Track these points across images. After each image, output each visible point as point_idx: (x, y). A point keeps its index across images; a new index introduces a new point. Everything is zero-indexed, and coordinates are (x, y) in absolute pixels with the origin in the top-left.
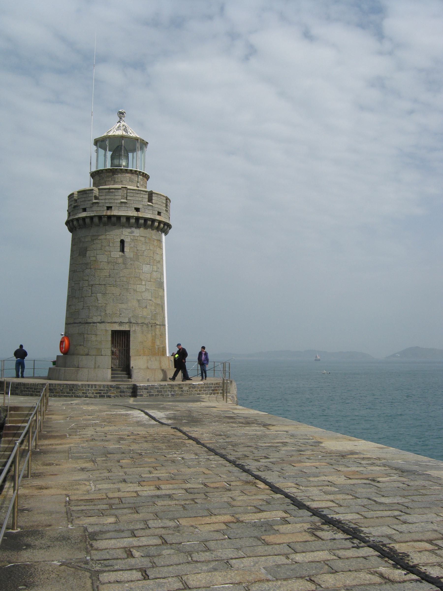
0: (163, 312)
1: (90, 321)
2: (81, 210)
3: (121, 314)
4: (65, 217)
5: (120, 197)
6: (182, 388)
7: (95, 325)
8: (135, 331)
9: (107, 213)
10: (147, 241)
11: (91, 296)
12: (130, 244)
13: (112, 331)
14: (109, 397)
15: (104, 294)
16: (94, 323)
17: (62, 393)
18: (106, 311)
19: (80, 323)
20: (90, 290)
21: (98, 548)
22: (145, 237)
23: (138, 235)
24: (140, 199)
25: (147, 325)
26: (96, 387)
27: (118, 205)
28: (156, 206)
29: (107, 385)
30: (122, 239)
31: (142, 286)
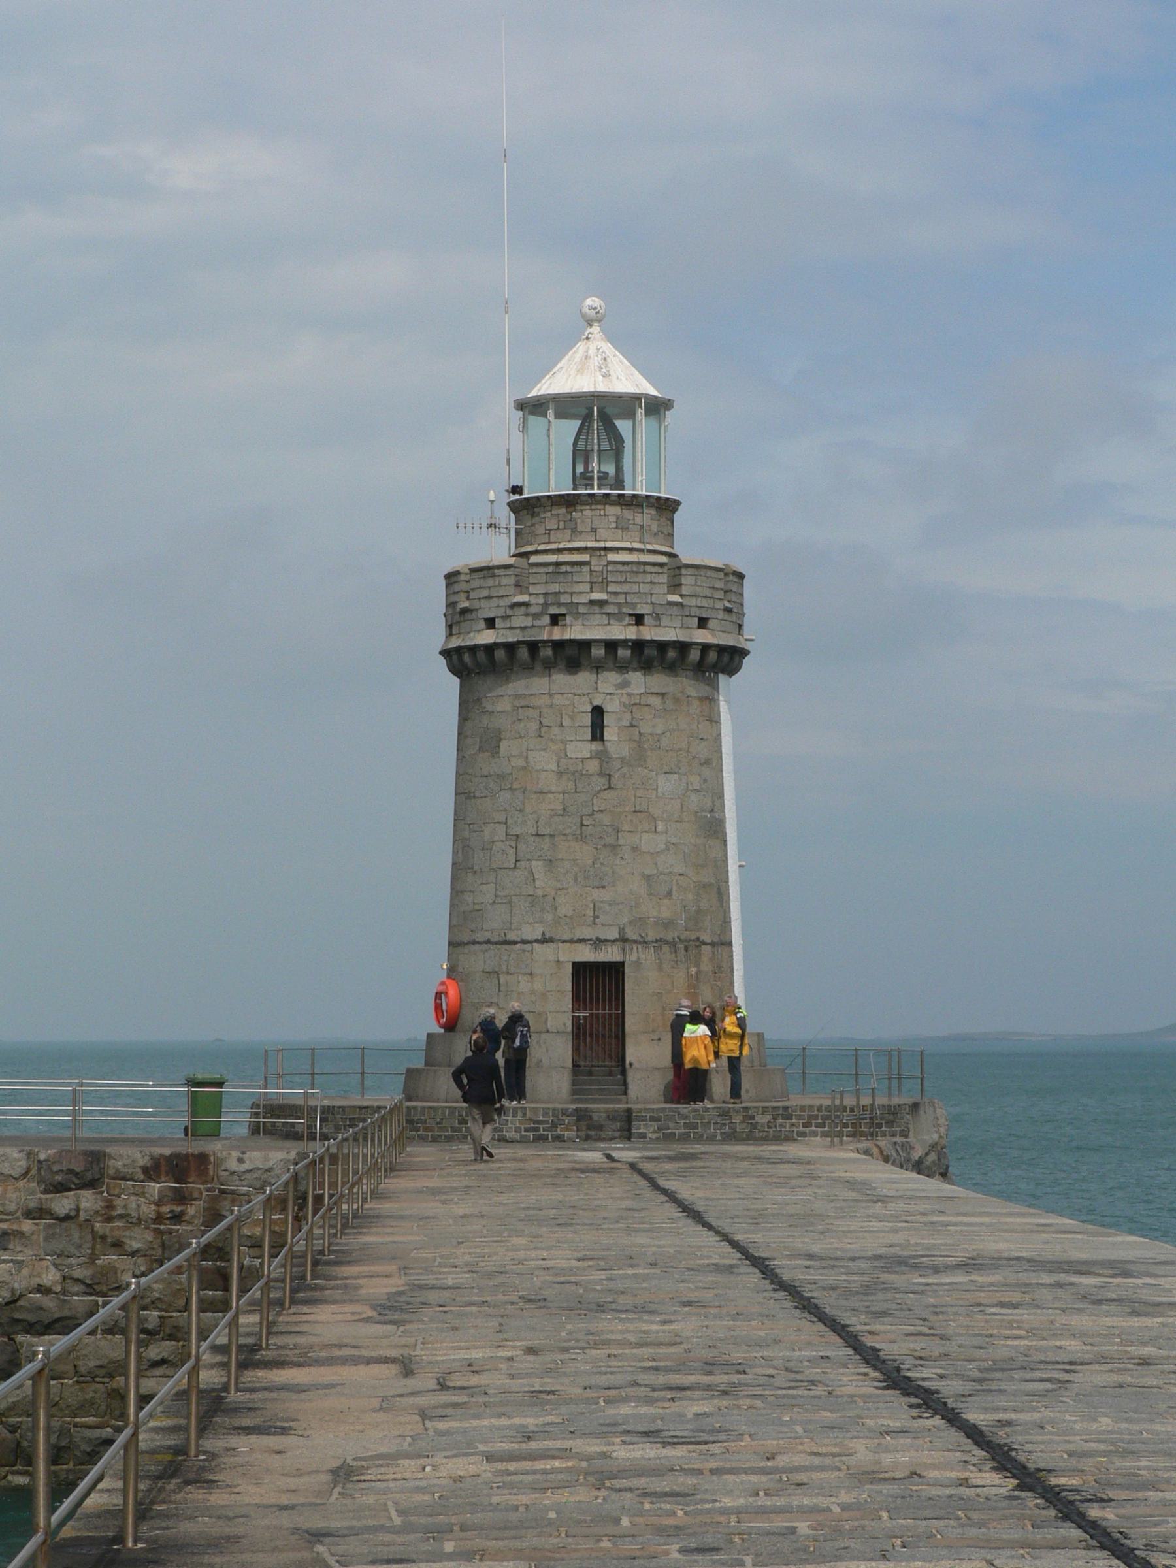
0: (722, 906)
2: (482, 624)
4: (437, 637)
5: (587, 588)
6: (753, 1118)
7: (528, 947)
8: (637, 964)
10: (670, 704)
11: (515, 867)
12: (620, 719)
13: (576, 965)
14: (559, 1139)
15: (550, 862)
16: (524, 942)
17: (441, 1129)
18: (556, 908)
19: (488, 942)
20: (512, 851)
22: (663, 695)
24: (644, 588)
25: (672, 944)
26: (524, 1114)
28: (692, 602)
29: (554, 1110)
30: (596, 703)
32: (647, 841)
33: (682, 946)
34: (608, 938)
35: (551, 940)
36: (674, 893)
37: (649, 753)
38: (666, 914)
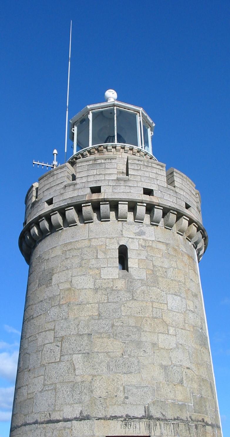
1: (58, 418)
3: (127, 398)
9: (91, 197)
10: (172, 253)
11: (60, 361)
15: (87, 355)
18: (92, 392)
19: (36, 423)
21: (112, 181)
22: (167, 244)
23: (153, 239)
24: (153, 176)
25: (186, 422)
27: (111, 183)
30: (121, 244)
31: (169, 337)
32: (163, 341)
33: (193, 425)
34: (136, 415)
35: (88, 418)
36: (185, 382)
37: (160, 279)
38: (180, 397)
